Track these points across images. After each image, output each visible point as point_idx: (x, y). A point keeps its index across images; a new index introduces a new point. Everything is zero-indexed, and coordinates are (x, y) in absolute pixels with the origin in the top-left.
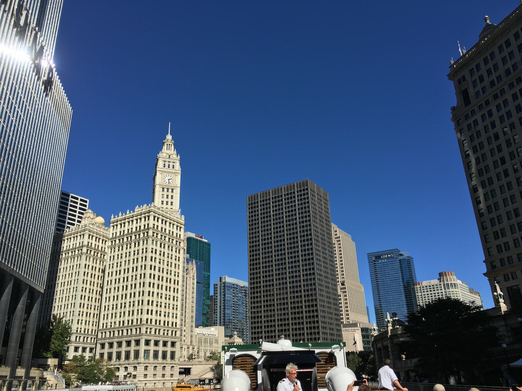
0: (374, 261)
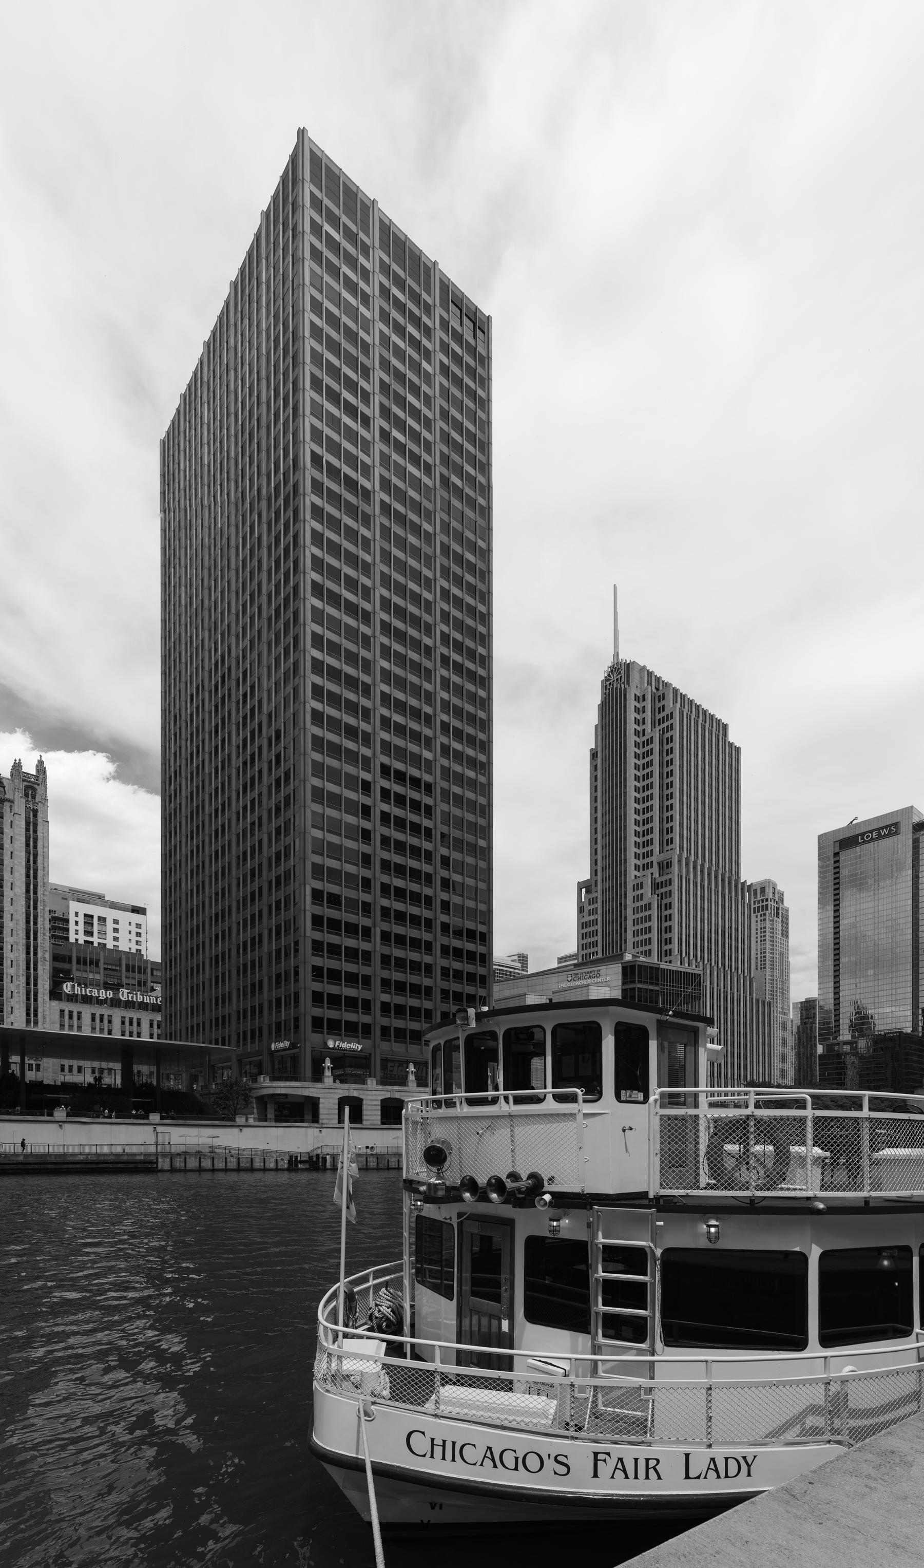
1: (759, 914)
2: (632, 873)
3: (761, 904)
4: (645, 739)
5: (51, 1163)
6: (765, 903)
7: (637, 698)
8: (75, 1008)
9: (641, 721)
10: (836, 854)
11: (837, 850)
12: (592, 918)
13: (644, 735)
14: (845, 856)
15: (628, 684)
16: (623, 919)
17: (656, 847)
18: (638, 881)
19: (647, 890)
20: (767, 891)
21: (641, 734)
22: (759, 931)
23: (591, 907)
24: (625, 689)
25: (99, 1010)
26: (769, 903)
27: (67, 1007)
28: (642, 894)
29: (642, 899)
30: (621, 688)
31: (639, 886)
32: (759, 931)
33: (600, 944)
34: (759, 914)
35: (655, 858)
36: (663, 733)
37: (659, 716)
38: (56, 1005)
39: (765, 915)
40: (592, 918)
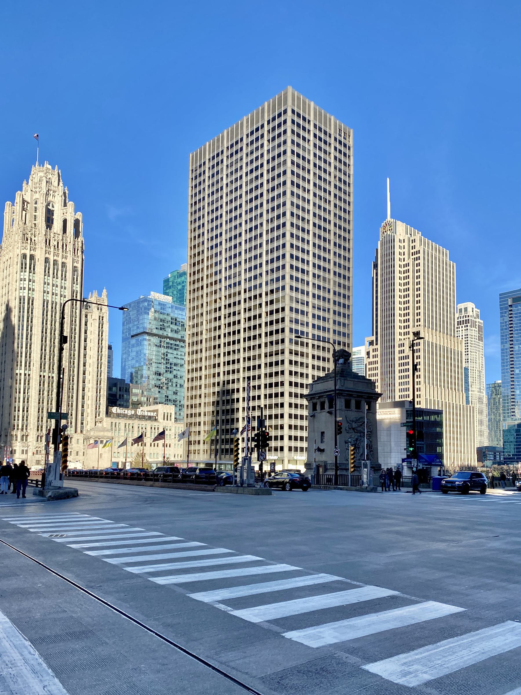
0: (511, 306)
1: (463, 326)
2: (397, 337)
3: (465, 319)
4: (405, 263)
5: (120, 489)
6: (467, 318)
7: (400, 241)
8: (117, 421)
9: (402, 247)
12: (374, 359)
13: (404, 261)
15: (396, 233)
16: (393, 366)
17: (411, 323)
18: (402, 342)
19: (406, 348)
20: (468, 310)
21: (402, 260)
22: (464, 337)
23: (374, 353)
24: (394, 236)
25: (128, 422)
26: (470, 318)
27: (114, 420)
28: (404, 350)
29: (404, 353)
30: (391, 235)
31: (403, 345)
32: (464, 337)
33: (379, 350)
34: (463, 326)
35: (411, 330)
36: (415, 261)
37: (411, 251)
38: (109, 420)
39: (467, 326)
40: (374, 359)
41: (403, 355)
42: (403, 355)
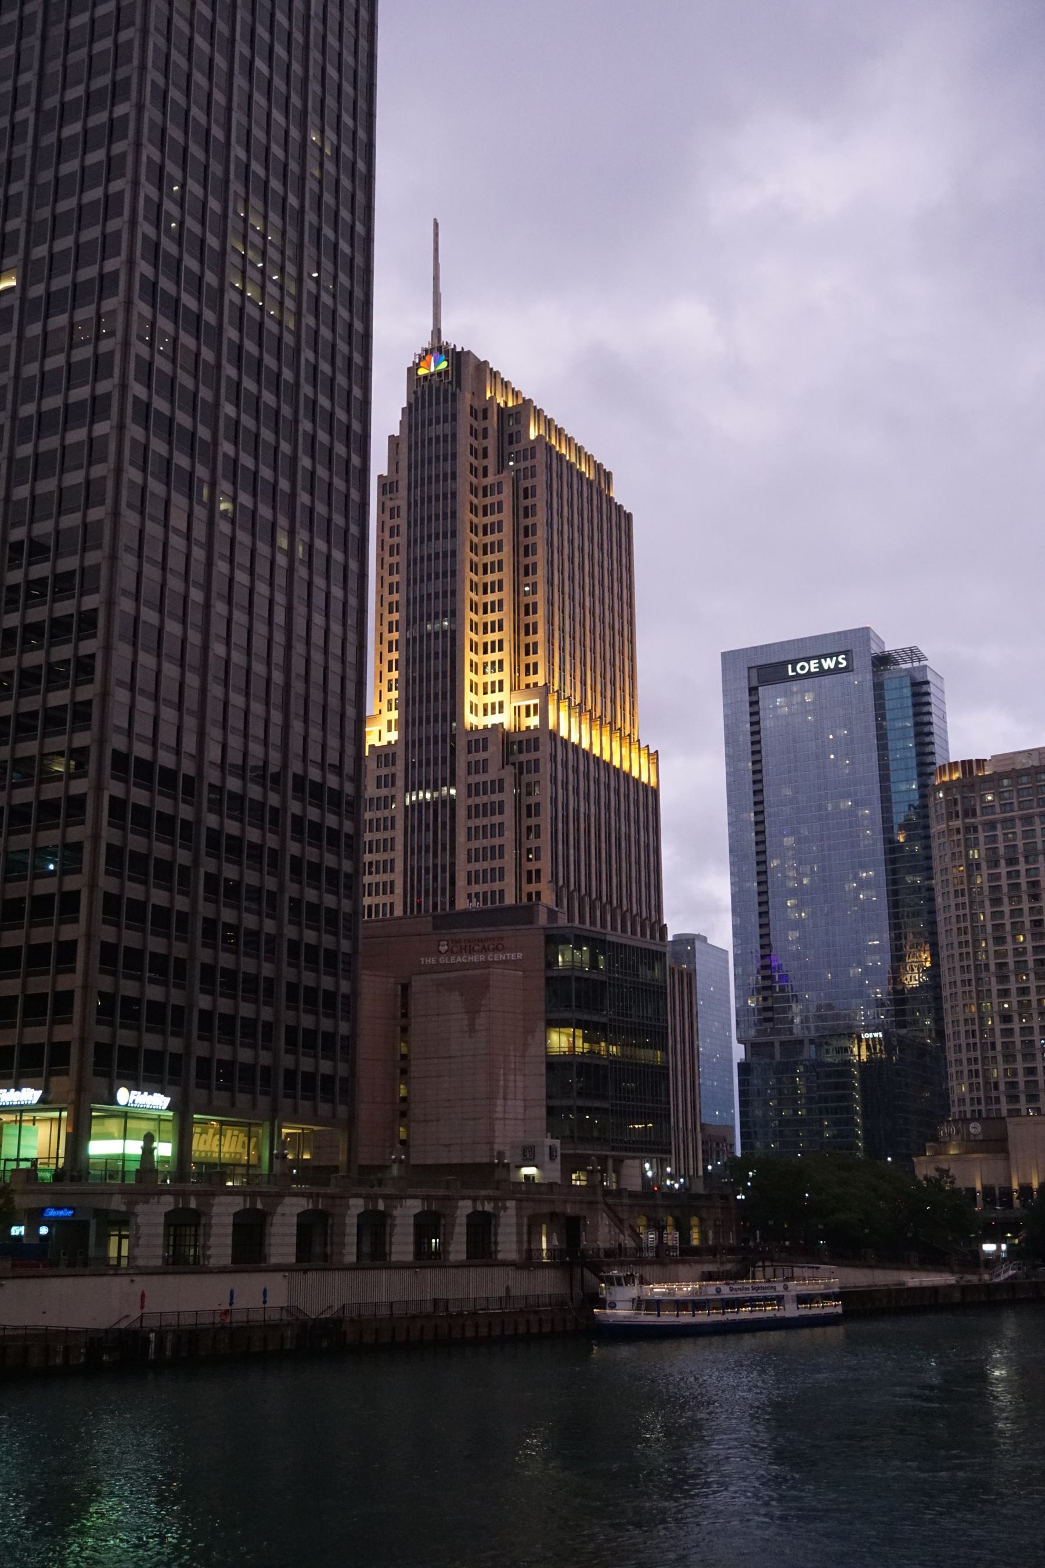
10: (753, 690)
11: (755, 683)
14: (764, 692)
41: (480, 778)
42: (480, 778)
